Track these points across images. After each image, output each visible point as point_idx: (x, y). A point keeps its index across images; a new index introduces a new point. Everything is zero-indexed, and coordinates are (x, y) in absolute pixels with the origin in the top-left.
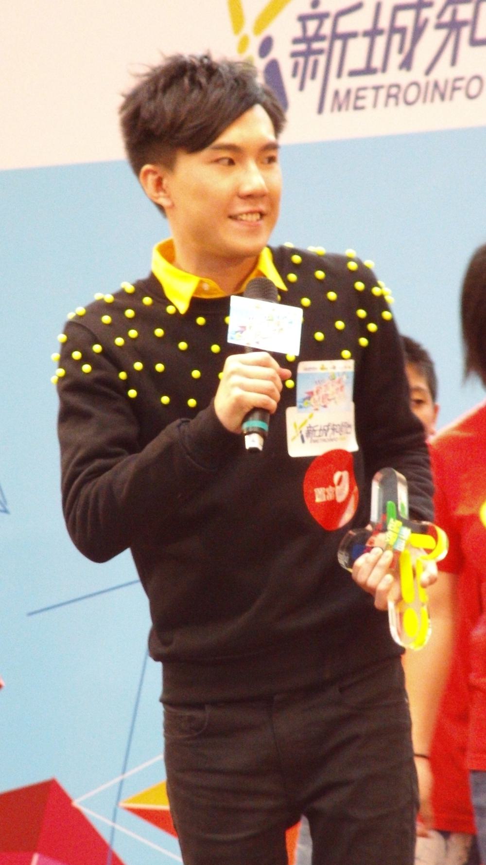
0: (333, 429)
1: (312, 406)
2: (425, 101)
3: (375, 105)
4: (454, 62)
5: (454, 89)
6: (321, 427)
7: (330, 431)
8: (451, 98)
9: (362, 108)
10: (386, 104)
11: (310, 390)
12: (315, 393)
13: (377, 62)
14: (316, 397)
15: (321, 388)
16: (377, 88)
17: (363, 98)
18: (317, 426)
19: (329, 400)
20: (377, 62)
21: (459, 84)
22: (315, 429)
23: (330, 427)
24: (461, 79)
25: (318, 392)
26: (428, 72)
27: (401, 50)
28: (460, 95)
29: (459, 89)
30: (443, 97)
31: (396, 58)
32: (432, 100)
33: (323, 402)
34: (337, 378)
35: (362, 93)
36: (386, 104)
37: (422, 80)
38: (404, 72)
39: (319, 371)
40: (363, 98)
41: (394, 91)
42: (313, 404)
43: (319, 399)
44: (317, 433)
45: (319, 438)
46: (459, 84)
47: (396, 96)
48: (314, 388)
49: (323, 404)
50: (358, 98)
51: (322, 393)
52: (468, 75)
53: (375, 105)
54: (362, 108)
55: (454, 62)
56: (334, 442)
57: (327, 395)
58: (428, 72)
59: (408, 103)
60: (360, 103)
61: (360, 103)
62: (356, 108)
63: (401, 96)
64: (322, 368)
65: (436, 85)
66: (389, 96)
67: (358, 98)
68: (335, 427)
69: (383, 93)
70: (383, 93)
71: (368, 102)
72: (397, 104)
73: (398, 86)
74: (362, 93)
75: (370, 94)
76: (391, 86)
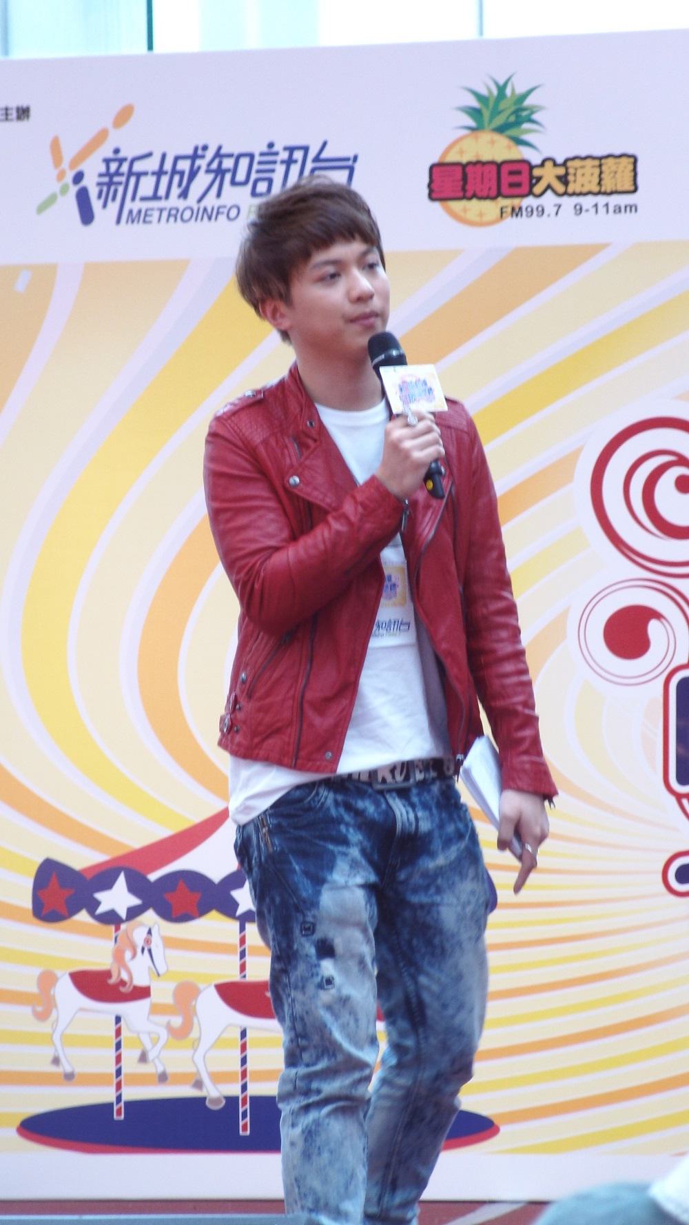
0: (220, 172)
2: (196, 219)
3: (159, 220)
4: (219, 195)
7: (202, 180)
8: (216, 218)
10: (168, 220)
24: (225, 207)
26: (200, 201)
28: (222, 218)
29: (223, 213)
30: (210, 218)
36: (168, 220)
50: (146, 215)
53: (159, 220)
54: (150, 222)
55: (219, 195)
58: (200, 201)
65: (205, 210)
66: (169, 215)
68: (228, 163)
69: (165, 214)
70: (165, 214)
75: (156, 214)
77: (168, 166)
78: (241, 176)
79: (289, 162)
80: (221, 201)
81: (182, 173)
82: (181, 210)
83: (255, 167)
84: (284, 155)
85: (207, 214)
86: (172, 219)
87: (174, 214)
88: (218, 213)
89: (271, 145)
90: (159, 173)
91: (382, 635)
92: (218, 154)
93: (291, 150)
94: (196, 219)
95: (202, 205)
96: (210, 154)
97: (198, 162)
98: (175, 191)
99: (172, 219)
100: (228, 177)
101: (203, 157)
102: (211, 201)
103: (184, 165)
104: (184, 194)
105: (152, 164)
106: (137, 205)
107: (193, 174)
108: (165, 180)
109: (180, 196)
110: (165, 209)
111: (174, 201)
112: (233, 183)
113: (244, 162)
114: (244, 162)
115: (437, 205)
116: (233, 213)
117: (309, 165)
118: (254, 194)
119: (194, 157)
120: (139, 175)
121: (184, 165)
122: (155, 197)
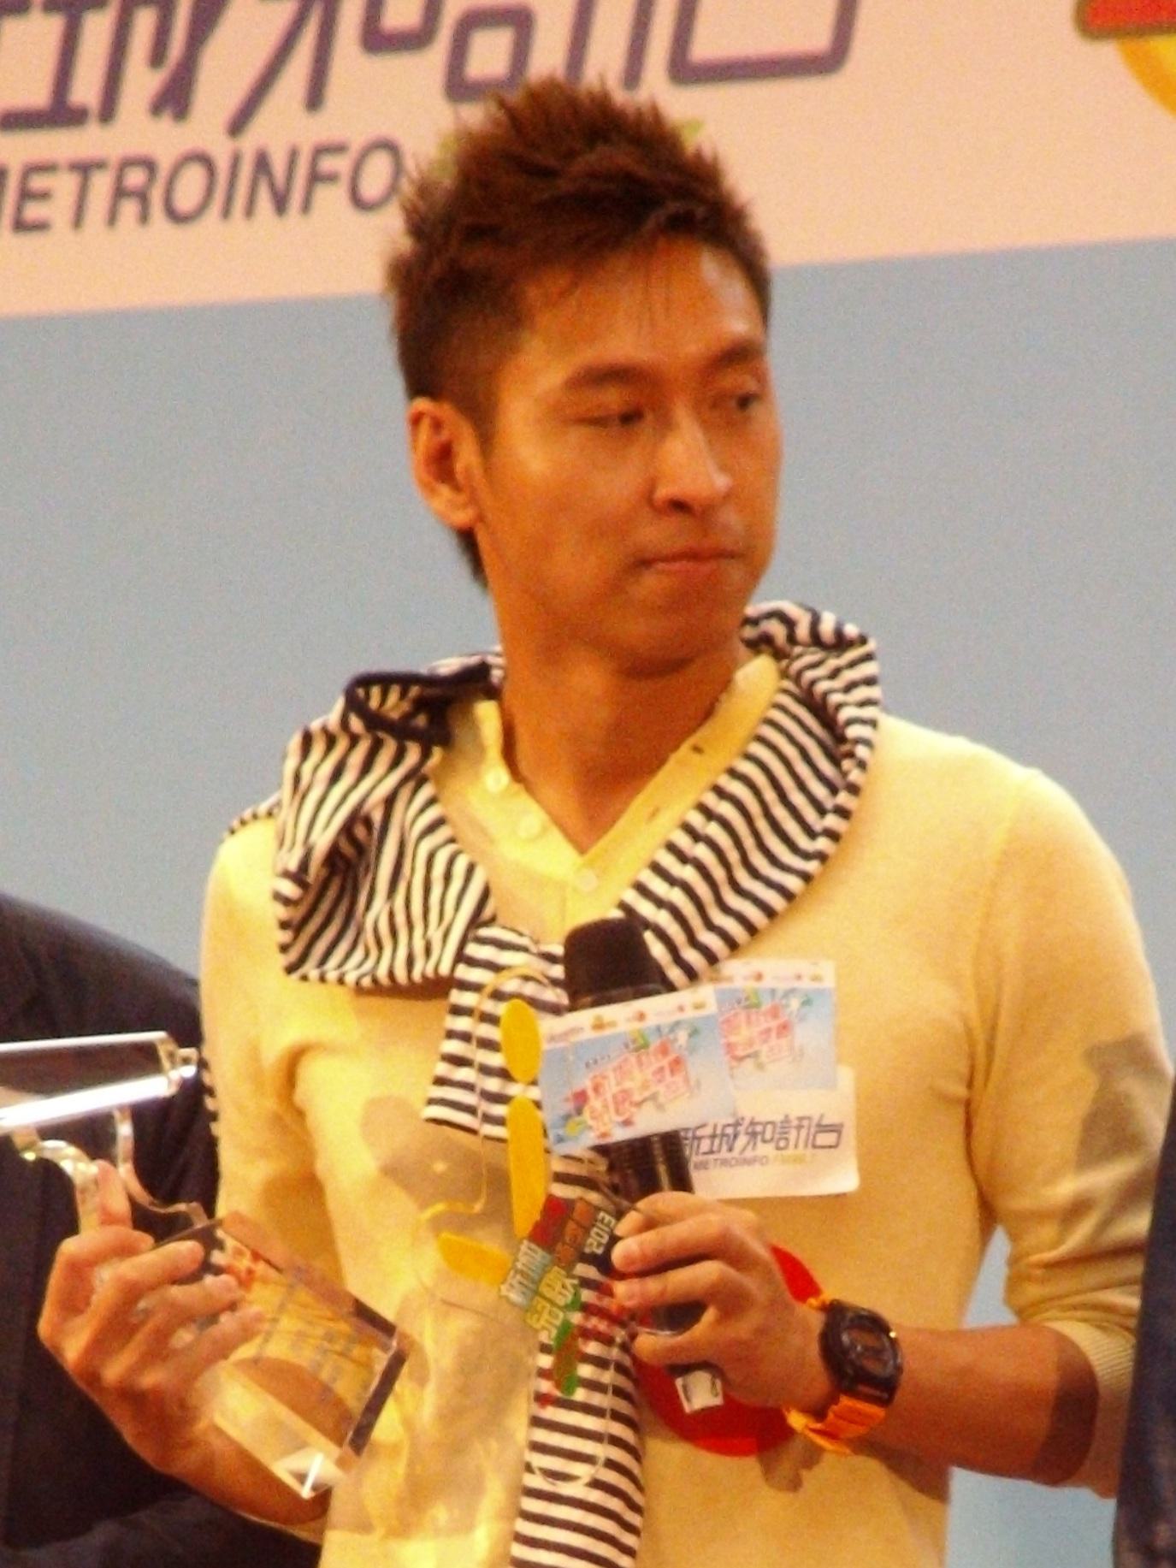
0: (754, 1135)
1: (590, 1128)
2: (226, 212)
3: (78, 220)
4: (315, 98)
5: (315, 178)
6: (715, 1127)
7: (742, 1140)
8: (306, 207)
9: (41, 226)
10: (112, 218)
11: (577, 1088)
12: (590, 1093)
13: (86, 89)
14: (595, 1103)
15: (604, 1077)
16: (84, 169)
17: (44, 196)
18: (703, 1126)
19: (639, 1104)
20: (86, 89)
21: (328, 164)
22: (699, 1133)
23: (741, 1129)
24: (339, 149)
25: (596, 1089)
26: (237, 125)
27: (157, 56)
28: (331, 198)
29: (332, 178)
30: (280, 203)
31: (142, 82)
32: (250, 211)
33: (617, 1112)
34: (767, 1005)
35: (38, 182)
36: (112, 218)
37: (221, 149)
38: (166, 123)
39: (589, 1034)
40: (44, 196)
41: (135, 178)
42: (591, 1122)
43: (606, 1106)
44: (705, 1145)
45: (711, 1157)
46: (328, 164)
47: (143, 197)
48: (586, 1083)
49: (620, 1119)
50: (26, 195)
51: (611, 1088)
52: (357, 140)
53: (78, 220)
54: (41, 226)
55: (315, 98)
56: (757, 1166)
57: (626, 1094)
58: (237, 125)
59: (175, 216)
60: (33, 211)
61: (33, 211)
62: (20, 226)
63: (156, 196)
64: (599, 1025)
65: (262, 163)
66: (120, 192)
67: (26, 195)
68: (759, 1128)
69: (101, 184)
70: (101, 184)
71: (58, 210)
72: (144, 217)
73: (149, 165)
74: (38, 182)
75: (64, 186)
76: (127, 163)
77: (719, 1132)
78: (768, 1136)
79: (799, 1127)
80: (322, 128)
81: (727, 1135)
82: (165, 165)
83: (778, 1130)
84: (795, 1123)
85: (272, 185)
86: (129, 208)
87: (725, 1162)
88: (315, 178)
89: (787, 1116)
90: (713, 1136)
91: (763, 1161)
92: (753, 1123)
93: (801, 1119)
94: (226, 212)
95: (249, 142)
96: (746, 1122)
97: (740, 1128)
98: (725, 1147)
99: (129, 208)
100: (759, 1137)
101: (741, 1125)
102: (749, 1154)
103: (730, 1131)
104: (730, 1149)
105: (708, 1131)
106: (701, 1158)
107: (736, 1136)
108: (717, 1141)
109: (157, 108)
110: (100, 165)
111: (724, 1154)
112: (764, 1141)
113: (769, 1127)
114: (769, 1127)
115: (1108, 53)
116: (764, 1160)
117: (813, 1130)
118: (458, 87)
119: (737, 1124)
120: (699, 1138)
121: (730, 1131)
122: (711, 1152)
